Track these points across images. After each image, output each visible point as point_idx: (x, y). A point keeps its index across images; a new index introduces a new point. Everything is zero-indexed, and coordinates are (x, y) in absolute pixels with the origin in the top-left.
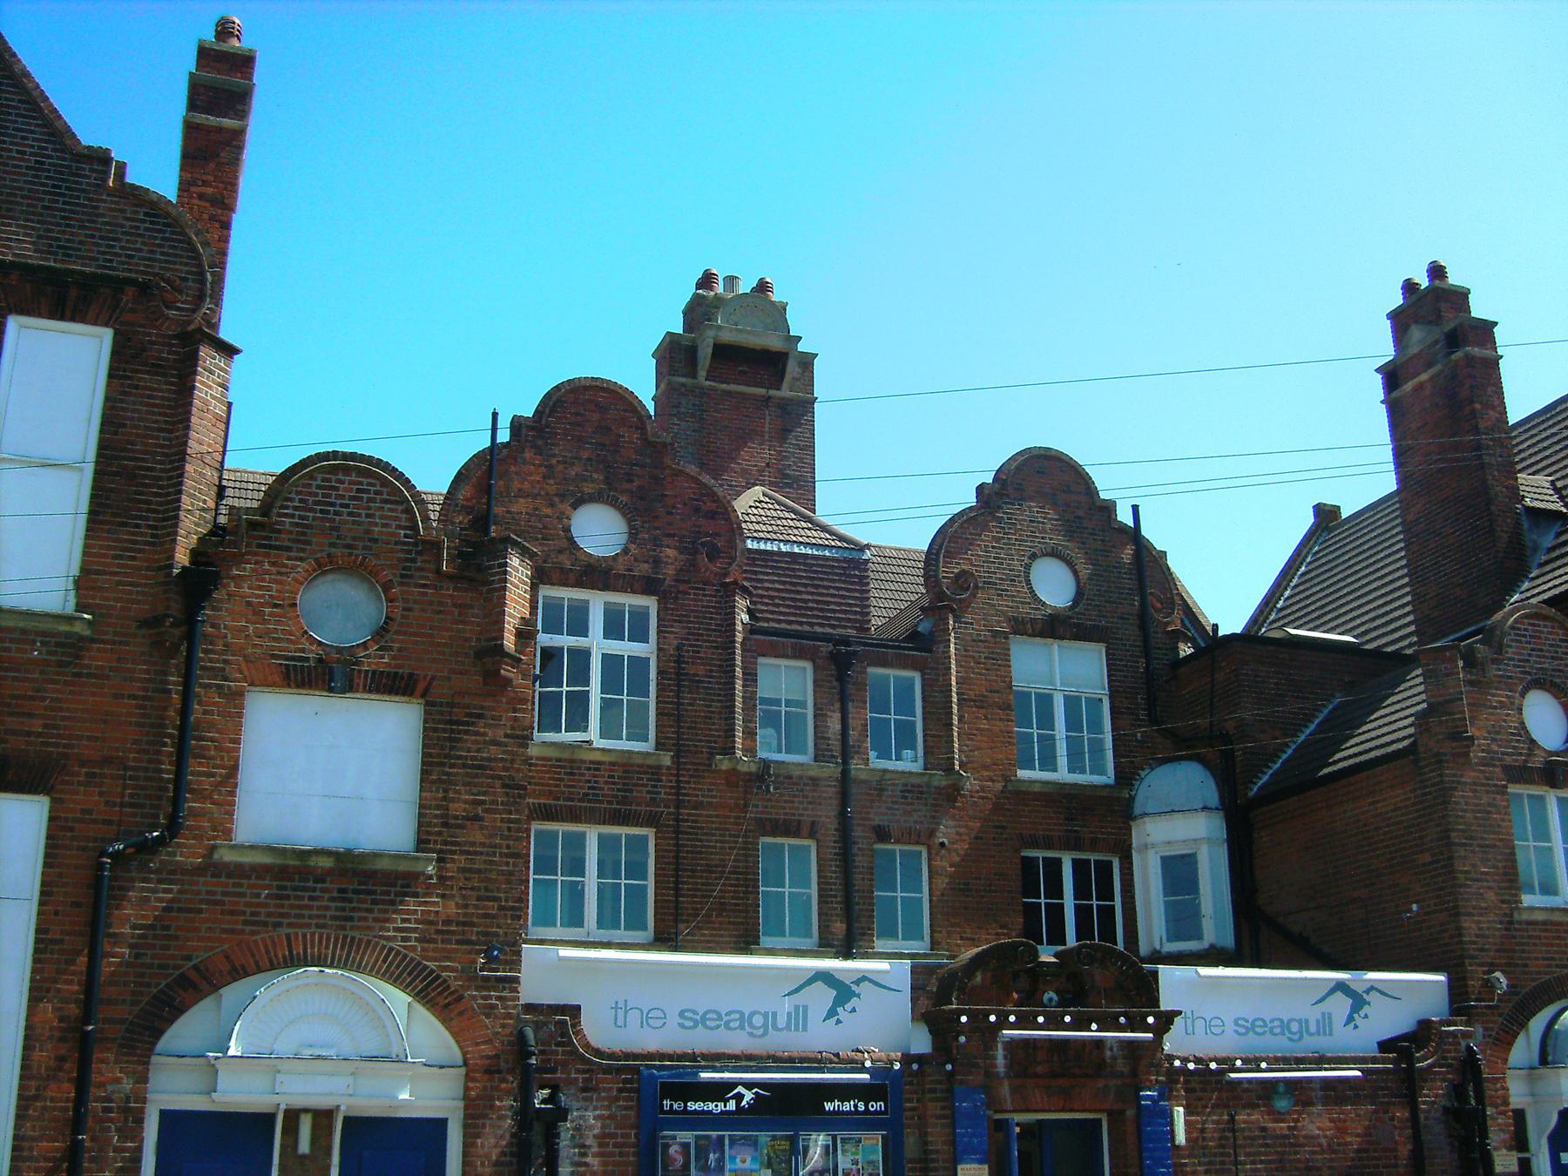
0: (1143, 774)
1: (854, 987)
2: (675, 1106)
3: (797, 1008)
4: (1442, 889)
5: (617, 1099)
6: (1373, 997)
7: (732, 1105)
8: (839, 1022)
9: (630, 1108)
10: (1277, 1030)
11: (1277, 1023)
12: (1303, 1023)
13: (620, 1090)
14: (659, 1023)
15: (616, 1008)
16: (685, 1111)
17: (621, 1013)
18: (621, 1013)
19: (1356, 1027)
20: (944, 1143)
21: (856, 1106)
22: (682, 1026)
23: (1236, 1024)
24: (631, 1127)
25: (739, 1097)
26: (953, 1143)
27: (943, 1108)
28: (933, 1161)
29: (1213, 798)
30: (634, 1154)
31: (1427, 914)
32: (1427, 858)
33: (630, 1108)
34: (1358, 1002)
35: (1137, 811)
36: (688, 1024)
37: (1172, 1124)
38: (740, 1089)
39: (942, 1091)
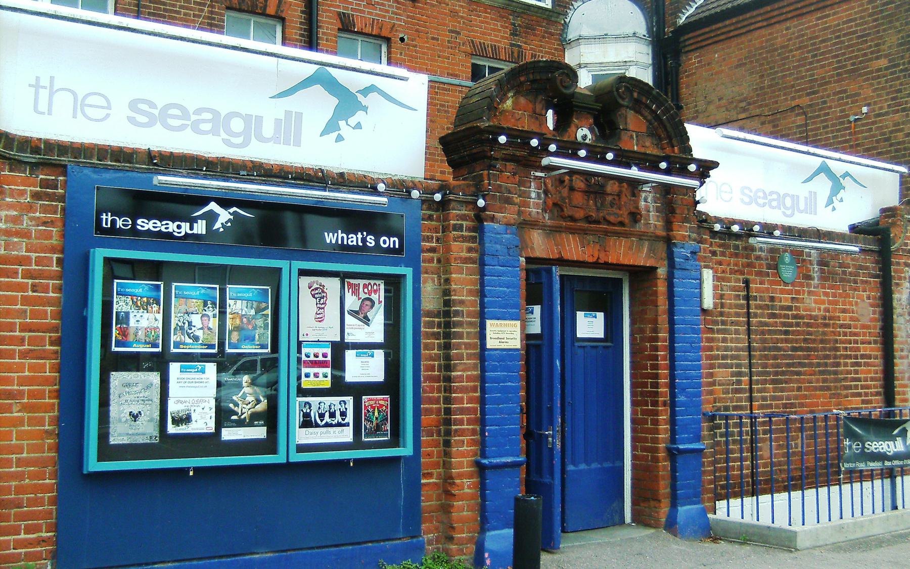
0: (576, 5)
1: (360, 97)
2: (120, 223)
3: (288, 114)
4: (900, 91)
5: (30, 208)
6: (847, 182)
7: (200, 228)
8: (340, 139)
9: (52, 223)
10: (774, 204)
11: (775, 196)
12: (795, 198)
13: (36, 196)
14: (101, 113)
15: (37, 86)
16: (134, 231)
17: (44, 94)
18: (44, 94)
19: (834, 209)
20: (470, 292)
21: (364, 240)
22: (131, 120)
23: (743, 193)
24: (53, 250)
25: (211, 217)
26: (482, 294)
27: (470, 250)
28: (457, 313)
29: (642, 30)
30: (52, 501)
31: (879, 115)
32: (883, 63)
33: (52, 223)
34: (837, 186)
35: (571, 35)
36: (143, 119)
37: (700, 286)
38: (213, 206)
39: (469, 229)
